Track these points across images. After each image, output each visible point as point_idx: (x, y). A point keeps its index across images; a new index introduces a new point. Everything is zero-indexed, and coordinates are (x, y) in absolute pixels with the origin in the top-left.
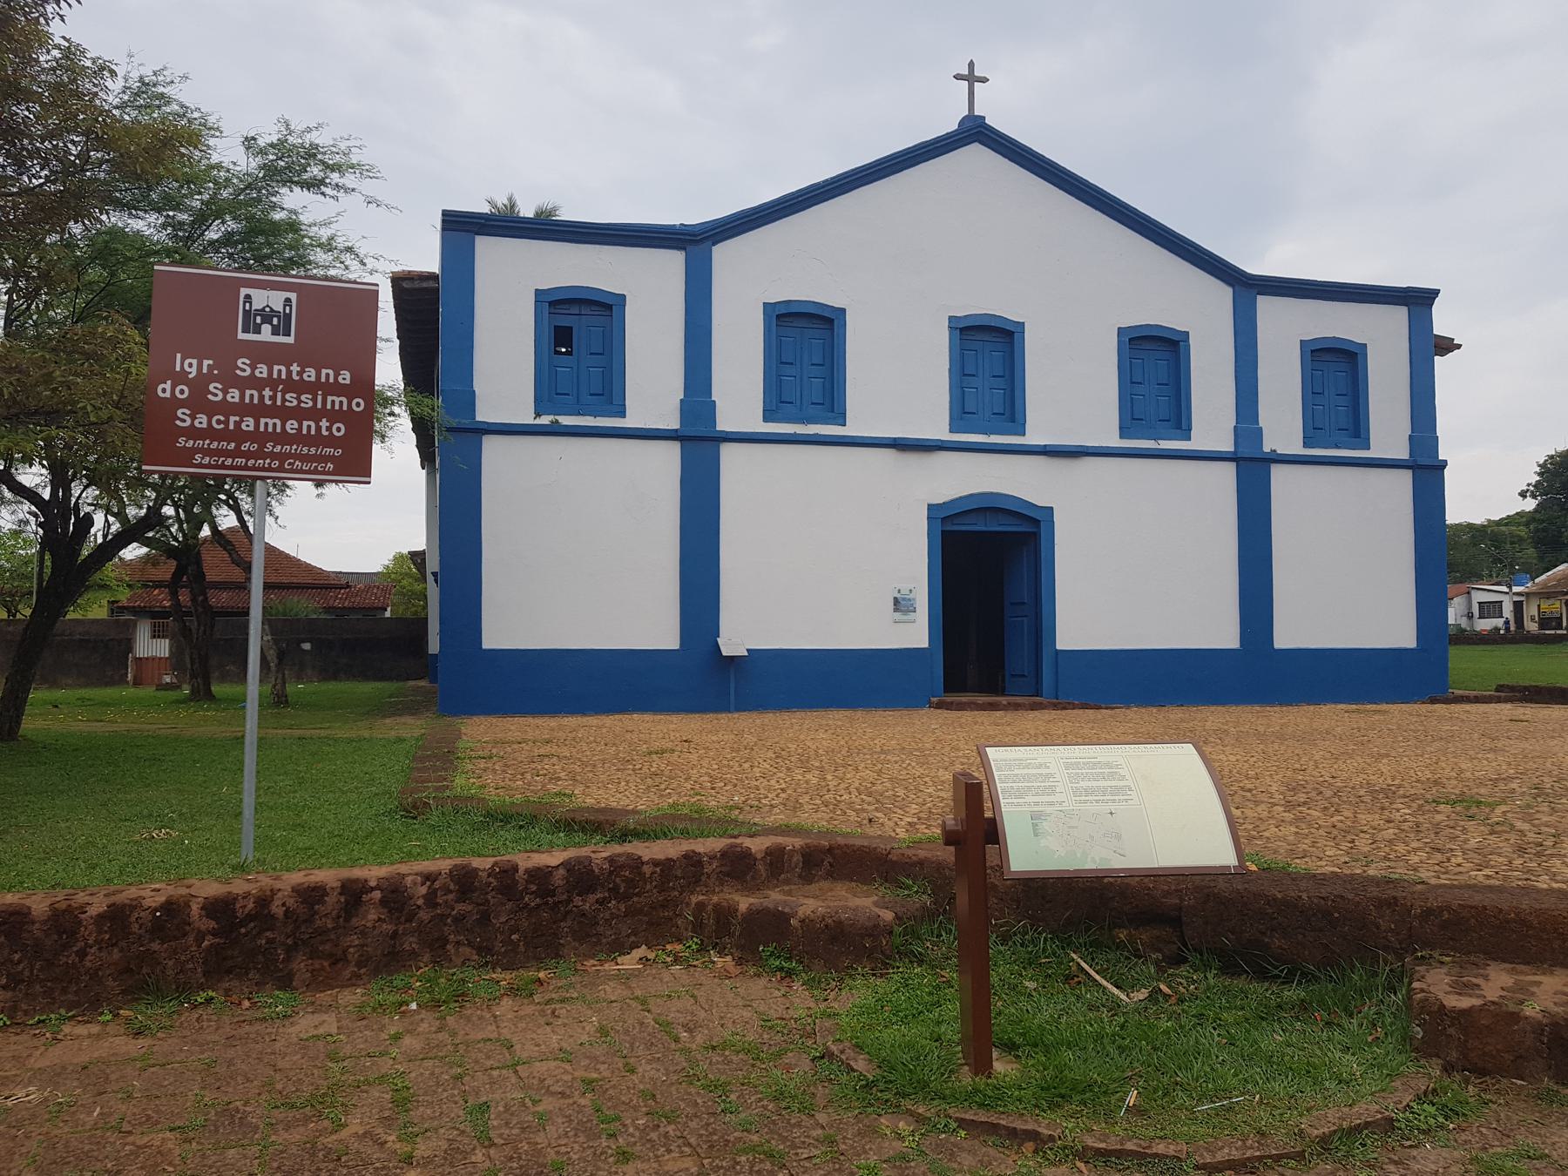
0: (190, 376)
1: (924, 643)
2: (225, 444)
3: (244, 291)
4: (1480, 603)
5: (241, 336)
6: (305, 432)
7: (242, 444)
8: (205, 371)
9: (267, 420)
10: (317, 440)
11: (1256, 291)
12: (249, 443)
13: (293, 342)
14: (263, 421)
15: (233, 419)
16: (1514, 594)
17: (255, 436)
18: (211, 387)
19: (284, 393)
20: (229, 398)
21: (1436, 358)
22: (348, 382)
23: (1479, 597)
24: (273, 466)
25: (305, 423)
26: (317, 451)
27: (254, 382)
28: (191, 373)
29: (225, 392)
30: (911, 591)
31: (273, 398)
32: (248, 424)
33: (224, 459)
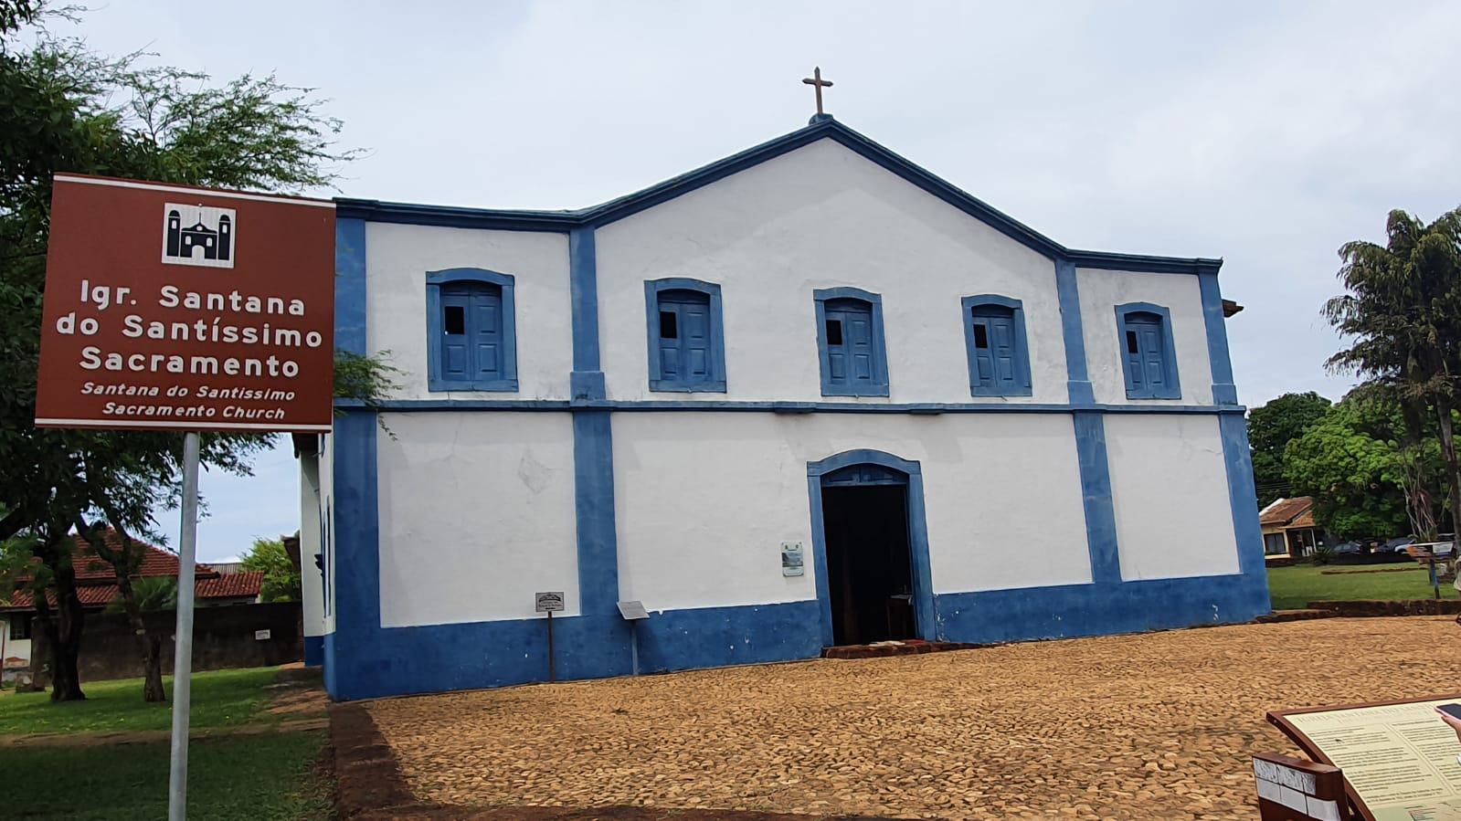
0: (100, 308)
1: (811, 595)
2: (146, 389)
3: (169, 207)
5: (167, 259)
6: (248, 372)
7: (168, 389)
8: (119, 301)
10: (265, 382)
11: (1074, 264)
12: (177, 387)
13: (232, 267)
14: (194, 360)
15: (155, 359)
17: (184, 379)
19: (221, 326)
20: (150, 333)
22: (301, 312)
24: (208, 414)
25: (249, 362)
26: (264, 395)
27: (182, 314)
28: (101, 304)
29: (146, 327)
30: (797, 546)
31: (208, 333)
32: (176, 365)
33: (144, 407)
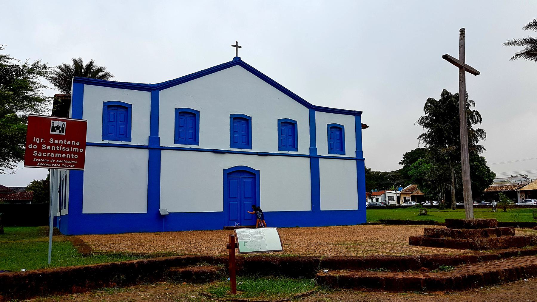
0: (37, 143)
3: (52, 121)
4: (388, 196)
6: (67, 157)
8: (41, 141)
9: (58, 154)
10: (70, 159)
14: (56, 154)
15: (48, 154)
16: (397, 194)
17: (54, 158)
18: (43, 146)
21: (362, 130)
22: (79, 145)
23: (388, 195)
27: (54, 144)
31: (59, 148)
32: (52, 155)
